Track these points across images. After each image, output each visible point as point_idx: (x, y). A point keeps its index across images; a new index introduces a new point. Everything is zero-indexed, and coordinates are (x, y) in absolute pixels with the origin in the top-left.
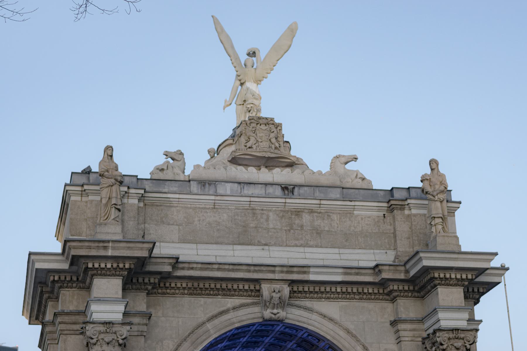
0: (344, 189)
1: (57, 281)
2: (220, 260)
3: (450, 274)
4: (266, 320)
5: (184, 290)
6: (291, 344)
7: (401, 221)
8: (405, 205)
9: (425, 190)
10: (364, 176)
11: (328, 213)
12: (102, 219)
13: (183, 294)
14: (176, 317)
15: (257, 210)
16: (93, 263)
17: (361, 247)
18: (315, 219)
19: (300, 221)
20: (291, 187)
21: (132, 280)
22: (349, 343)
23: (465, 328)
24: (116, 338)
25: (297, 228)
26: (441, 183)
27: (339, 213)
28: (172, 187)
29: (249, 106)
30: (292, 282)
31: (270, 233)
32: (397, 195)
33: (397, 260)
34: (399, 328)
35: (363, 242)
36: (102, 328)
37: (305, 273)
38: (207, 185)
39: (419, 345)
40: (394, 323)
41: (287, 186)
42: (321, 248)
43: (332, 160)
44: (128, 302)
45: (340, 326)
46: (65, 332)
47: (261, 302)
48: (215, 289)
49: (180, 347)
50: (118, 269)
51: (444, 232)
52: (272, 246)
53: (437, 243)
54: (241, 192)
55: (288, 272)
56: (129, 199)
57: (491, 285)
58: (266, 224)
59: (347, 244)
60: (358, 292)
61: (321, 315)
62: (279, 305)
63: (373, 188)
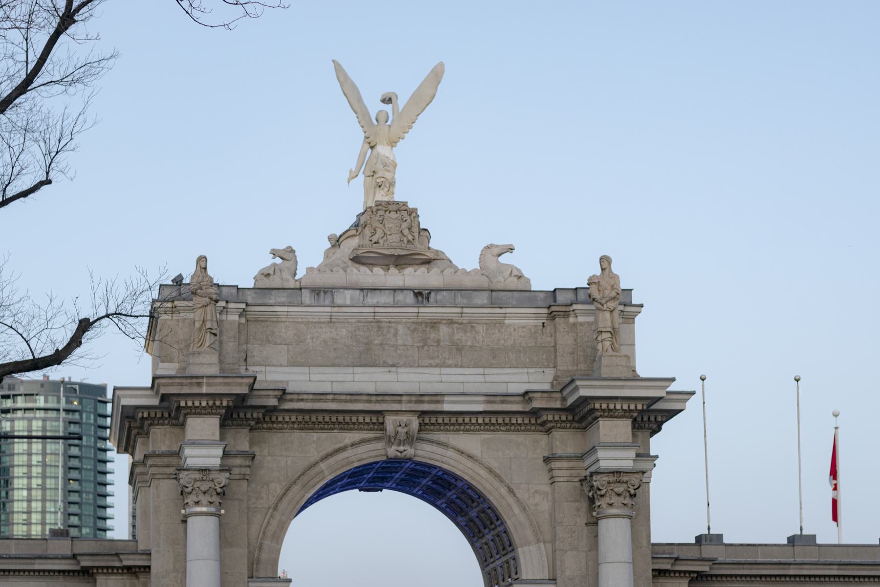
0: (493, 292)
1: (146, 419)
2: (337, 388)
3: (615, 404)
4: (391, 459)
5: (293, 424)
6: (426, 480)
7: (563, 332)
8: (569, 311)
10: (522, 273)
11: (472, 323)
12: (196, 346)
13: (293, 429)
15: (384, 323)
16: (186, 401)
17: (512, 366)
18: (455, 331)
22: (491, 484)
24: (213, 486)
25: (432, 344)
26: (613, 288)
27: (486, 323)
28: (280, 297)
29: (378, 180)
30: (423, 413)
31: (399, 352)
32: (561, 298)
33: (556, 381)
34: (553, 467)
35: (514, 359)
36: (197, 476)
37: (438, 402)
38: (322, 294)
39: (576, 487)
40: (547, 460)
42: (461, 368)
43: (482, 251)
44: (226, 445)
45: (481, 464)
46: (158, 476)
48: (330, 423)
50: (214, 408)
51: (613, 350)
52: (400, 367)
54: (364, 300)
55: (417, 402)
56: (228, 315)
58: (393, 340)
61: (458, 451)
63: (531, 288)
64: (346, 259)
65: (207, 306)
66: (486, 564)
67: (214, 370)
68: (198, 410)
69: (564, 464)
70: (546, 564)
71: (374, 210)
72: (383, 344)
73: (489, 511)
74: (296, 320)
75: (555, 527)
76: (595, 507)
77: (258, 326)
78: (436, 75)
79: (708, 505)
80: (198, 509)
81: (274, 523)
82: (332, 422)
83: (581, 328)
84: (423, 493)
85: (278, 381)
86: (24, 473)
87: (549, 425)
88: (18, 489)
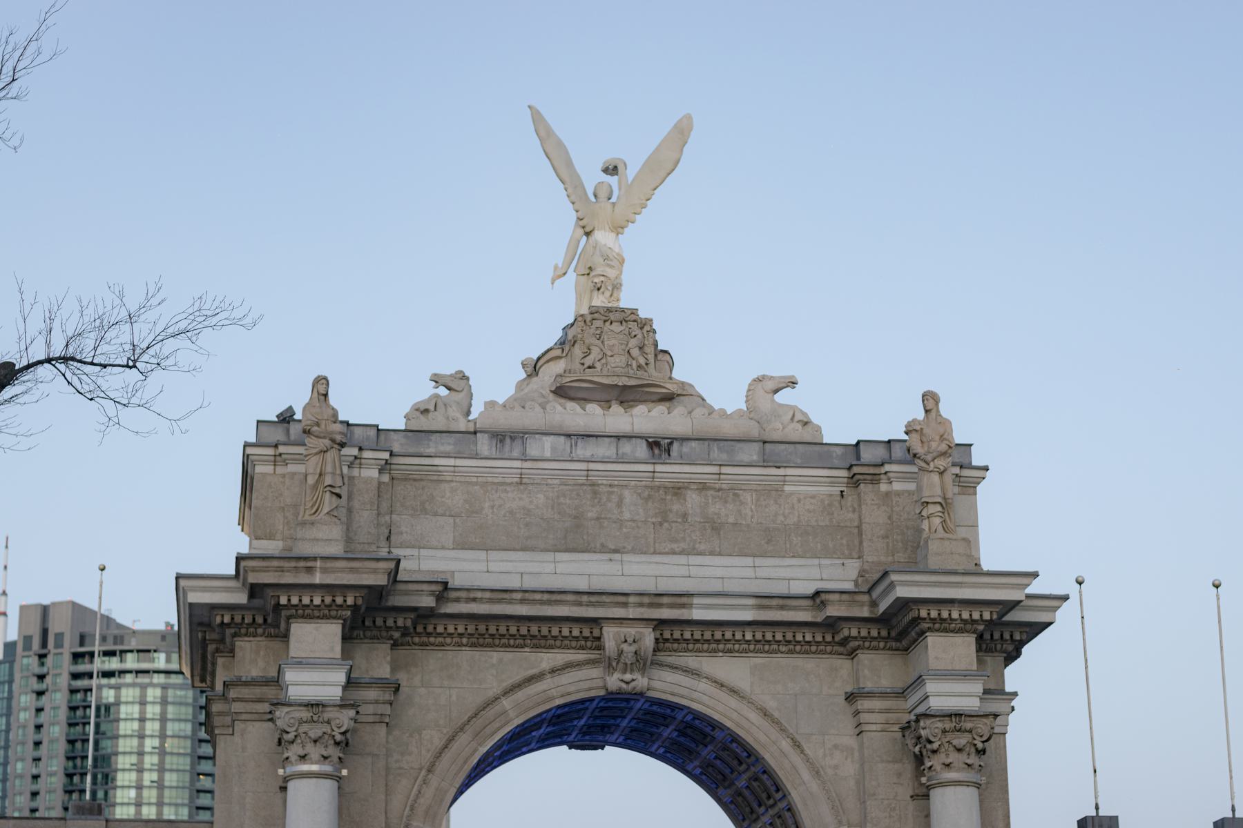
0: (766, 444)
1: (228, 625)
2: (529, 583)
3: (950, 611)
4: (612, 693)
5: (461, 638)
6: (669, 731)
7: (872, 504)
8: (880, 474)
9: (913, 450)
12: (308, 512)
13: (461, 645)
14: (446, 687)
16: (289, 596)
18: (710, 501)
19: (682, 506)
20: (666, 441)
21: (363, 622)
23: (976, 711)
24: (329, 731)
25: (675, 519)
26: (942, 438)
27: (756, 490)
28: (443, 444)
29: (596, 280)
30: (660, 624)
32: (867, 455)
34: (859, 708)
35: (799, 545)
36: (305, 714)
37: (683, 606)
38: (508, 441)
39: (896, 739)
40: (851, 697)
41: (659, 440)
42: (719, 557)
43: (750, 385)
44: (351, 666)
46: (244, 717)
47: (603, 660)
48: (518, 636)
49: (453, 742)
50: (334, 607)
53: (928, 552)
54: (571, 452)
56: (362, 470)
57: (1037, 629)
59: (769, 549)
60: (784, 639)
61: (715, 682)
62: (634, 665)
64: (546, 392)
65: (327, 451)
67: (336, 549)
68: (307, 612)
69: (877, 704)
71: (589, 318)
72: (601, 518)
74: (467, 479)
75: (864, 802)
76: (924, 770)
77: (409, 487)
78: (681, 132)
79: (1095, 771)
80: (305, 767)
82: (520, 635)
83: (898, 499)
84: (666, 752)
85: (437, 571)
86: (132, 765)
88: (123, 787)
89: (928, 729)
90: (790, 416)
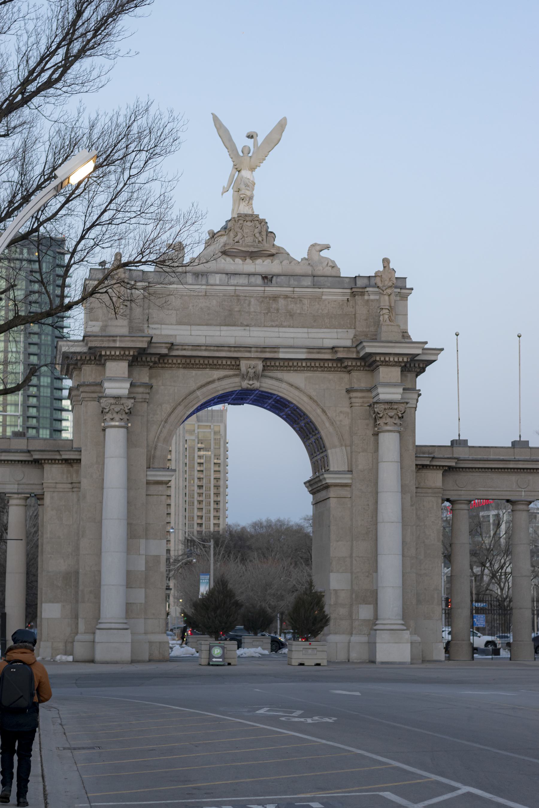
13: (179, 368)
21: (137, 359)
29: (242, 196)
30: (266, 359)
32: (360, 283)
36: (112, 401)
37: (275, 352)
38: (200, 276)
40: (348, 391)
45: (304, 393)
46: (86, 399)
55: (261, 352)
57: (431, 362)
66: (312, 456)
67: (125, 331)
69: (359, 394)
70: (346, 460)
71: (236, 220)
73: (311, 424)
78: (282, 126)
80: (113, 423)
81: (165, 431)
87: (349, 368)
89: (378, 408)
90: (326, 264)
